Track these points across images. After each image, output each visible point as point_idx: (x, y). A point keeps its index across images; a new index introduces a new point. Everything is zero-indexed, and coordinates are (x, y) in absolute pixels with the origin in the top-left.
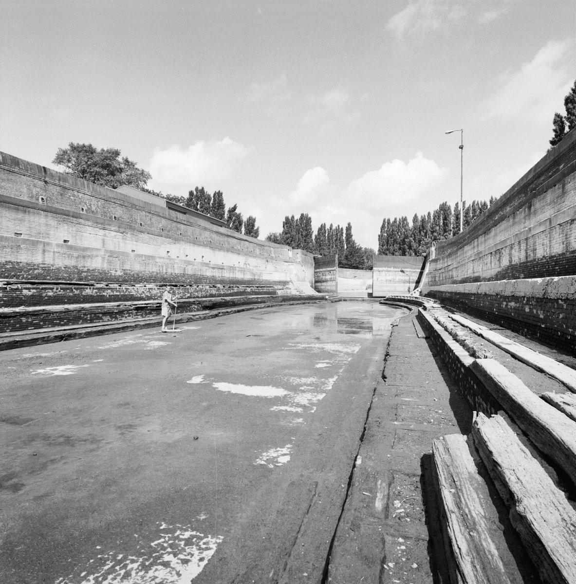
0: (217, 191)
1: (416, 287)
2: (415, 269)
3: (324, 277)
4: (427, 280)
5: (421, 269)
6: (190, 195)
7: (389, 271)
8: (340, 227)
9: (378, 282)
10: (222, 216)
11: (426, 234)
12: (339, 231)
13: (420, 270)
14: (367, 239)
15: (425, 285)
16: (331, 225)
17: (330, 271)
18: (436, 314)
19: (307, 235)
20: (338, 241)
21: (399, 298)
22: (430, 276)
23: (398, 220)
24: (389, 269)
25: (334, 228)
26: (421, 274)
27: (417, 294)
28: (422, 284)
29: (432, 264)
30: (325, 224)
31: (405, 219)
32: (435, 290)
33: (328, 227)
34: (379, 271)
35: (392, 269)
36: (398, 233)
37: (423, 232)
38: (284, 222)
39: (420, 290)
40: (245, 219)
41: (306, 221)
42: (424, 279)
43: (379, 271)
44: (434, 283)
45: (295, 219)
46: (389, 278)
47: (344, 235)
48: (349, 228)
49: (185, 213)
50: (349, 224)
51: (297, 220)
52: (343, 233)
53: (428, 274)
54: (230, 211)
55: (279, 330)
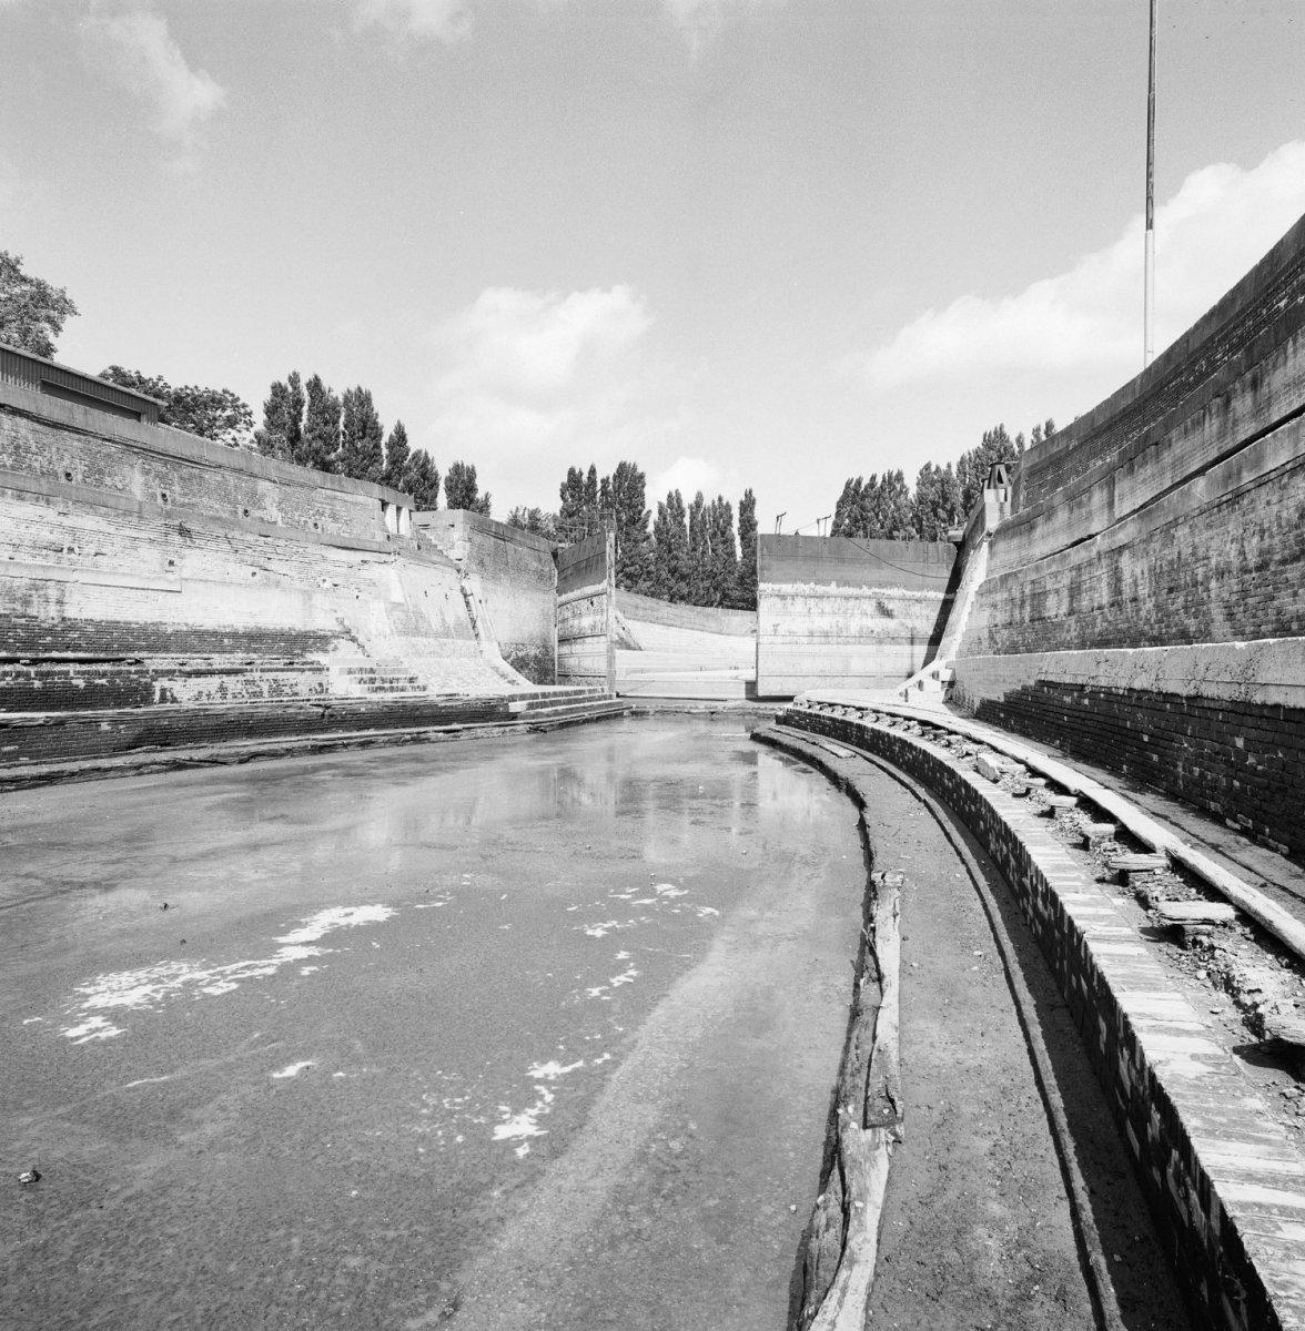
0: (353, 390)
1: (929, 658)
2: (921, 588)
3: (576, 622)
4: (984, 619)
5: (947, 592)
6: (275, 394)
7: (821, 597)
8: (724, 503)
9: (779, 639)
10: (374, 457)
11: (951, 513)
12: (723, 509)
13: (941, 596)
14: (800, 506)
15: (972, 647)
16: (700, 497)
17: (590, 598)
18: (1002, 767)
19: (633, 521)
20: (719, 538)
21: (838, 714)
22: (1000, 597)
23: (879, 481)
24: (821, 589)
25: (707, 503)
26: (947, 606)
27: (929, 703)
28: (952, 644)
29: (1001, 546)
30: (677, 491)
31: (899, 477)
32: (1121, 681)
33: (688, 500)
34: (783, 597)
35: (832, 588)
36: (877, 515)
37: (943, 508)
38: (562, 484)
39: (946, 676)
40: (443, 470)
41: (629, 482)
42: (965, 617)
43: (783, 597)
44: (1033, 632)
45: (599, 477)
46: (823, 623)
47: (736, 524)
48: (748, 505)
49: (137, 416)
50: (749, 494)
51: (605, 482)
52: (731, 517)
53: (986, 590)
54: (390, 446)
55: (373, 825)
